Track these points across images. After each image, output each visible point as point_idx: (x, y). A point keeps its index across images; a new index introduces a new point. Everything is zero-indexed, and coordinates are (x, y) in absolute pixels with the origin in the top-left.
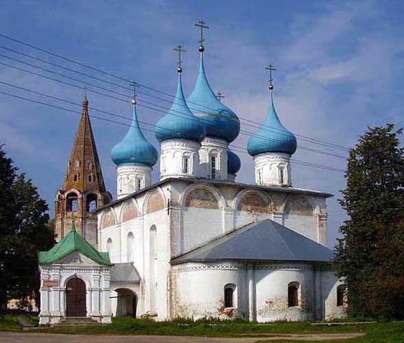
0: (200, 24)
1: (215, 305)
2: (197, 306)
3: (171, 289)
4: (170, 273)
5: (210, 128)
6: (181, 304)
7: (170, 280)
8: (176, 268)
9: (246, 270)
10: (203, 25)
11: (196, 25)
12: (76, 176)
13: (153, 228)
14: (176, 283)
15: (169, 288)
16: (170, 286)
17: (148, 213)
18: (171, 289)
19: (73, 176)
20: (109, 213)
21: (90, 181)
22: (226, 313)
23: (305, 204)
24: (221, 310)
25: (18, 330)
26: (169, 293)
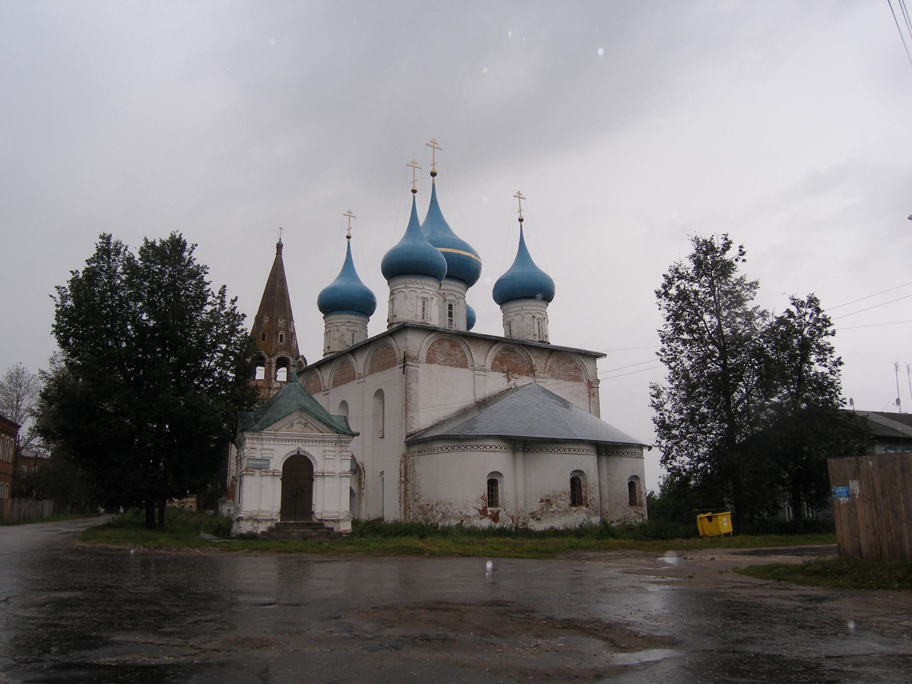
0: (518, 195)
1: (475, 505)
2: (449, 505)
3: (406, 480)
4: (404, 456)
5: (514, 452)
6: (422, 503)
7: (406, 468)
8: (414, 449)
9: (514, 453)
10: (521, 196)
11: (514, 196)
12: (264, 335)
13: (380, 394)
14: (414, 472)
15: (403, 479)
16: (405, 476)
17: (372, 372)
18: (406, 480)
19: (261, 334)
20: (313, 377)
21: (281, 341)
22: (490, 517)
23: (572, 365)
24: (483, 512)
25: (295, 340)
26: (403, 486)
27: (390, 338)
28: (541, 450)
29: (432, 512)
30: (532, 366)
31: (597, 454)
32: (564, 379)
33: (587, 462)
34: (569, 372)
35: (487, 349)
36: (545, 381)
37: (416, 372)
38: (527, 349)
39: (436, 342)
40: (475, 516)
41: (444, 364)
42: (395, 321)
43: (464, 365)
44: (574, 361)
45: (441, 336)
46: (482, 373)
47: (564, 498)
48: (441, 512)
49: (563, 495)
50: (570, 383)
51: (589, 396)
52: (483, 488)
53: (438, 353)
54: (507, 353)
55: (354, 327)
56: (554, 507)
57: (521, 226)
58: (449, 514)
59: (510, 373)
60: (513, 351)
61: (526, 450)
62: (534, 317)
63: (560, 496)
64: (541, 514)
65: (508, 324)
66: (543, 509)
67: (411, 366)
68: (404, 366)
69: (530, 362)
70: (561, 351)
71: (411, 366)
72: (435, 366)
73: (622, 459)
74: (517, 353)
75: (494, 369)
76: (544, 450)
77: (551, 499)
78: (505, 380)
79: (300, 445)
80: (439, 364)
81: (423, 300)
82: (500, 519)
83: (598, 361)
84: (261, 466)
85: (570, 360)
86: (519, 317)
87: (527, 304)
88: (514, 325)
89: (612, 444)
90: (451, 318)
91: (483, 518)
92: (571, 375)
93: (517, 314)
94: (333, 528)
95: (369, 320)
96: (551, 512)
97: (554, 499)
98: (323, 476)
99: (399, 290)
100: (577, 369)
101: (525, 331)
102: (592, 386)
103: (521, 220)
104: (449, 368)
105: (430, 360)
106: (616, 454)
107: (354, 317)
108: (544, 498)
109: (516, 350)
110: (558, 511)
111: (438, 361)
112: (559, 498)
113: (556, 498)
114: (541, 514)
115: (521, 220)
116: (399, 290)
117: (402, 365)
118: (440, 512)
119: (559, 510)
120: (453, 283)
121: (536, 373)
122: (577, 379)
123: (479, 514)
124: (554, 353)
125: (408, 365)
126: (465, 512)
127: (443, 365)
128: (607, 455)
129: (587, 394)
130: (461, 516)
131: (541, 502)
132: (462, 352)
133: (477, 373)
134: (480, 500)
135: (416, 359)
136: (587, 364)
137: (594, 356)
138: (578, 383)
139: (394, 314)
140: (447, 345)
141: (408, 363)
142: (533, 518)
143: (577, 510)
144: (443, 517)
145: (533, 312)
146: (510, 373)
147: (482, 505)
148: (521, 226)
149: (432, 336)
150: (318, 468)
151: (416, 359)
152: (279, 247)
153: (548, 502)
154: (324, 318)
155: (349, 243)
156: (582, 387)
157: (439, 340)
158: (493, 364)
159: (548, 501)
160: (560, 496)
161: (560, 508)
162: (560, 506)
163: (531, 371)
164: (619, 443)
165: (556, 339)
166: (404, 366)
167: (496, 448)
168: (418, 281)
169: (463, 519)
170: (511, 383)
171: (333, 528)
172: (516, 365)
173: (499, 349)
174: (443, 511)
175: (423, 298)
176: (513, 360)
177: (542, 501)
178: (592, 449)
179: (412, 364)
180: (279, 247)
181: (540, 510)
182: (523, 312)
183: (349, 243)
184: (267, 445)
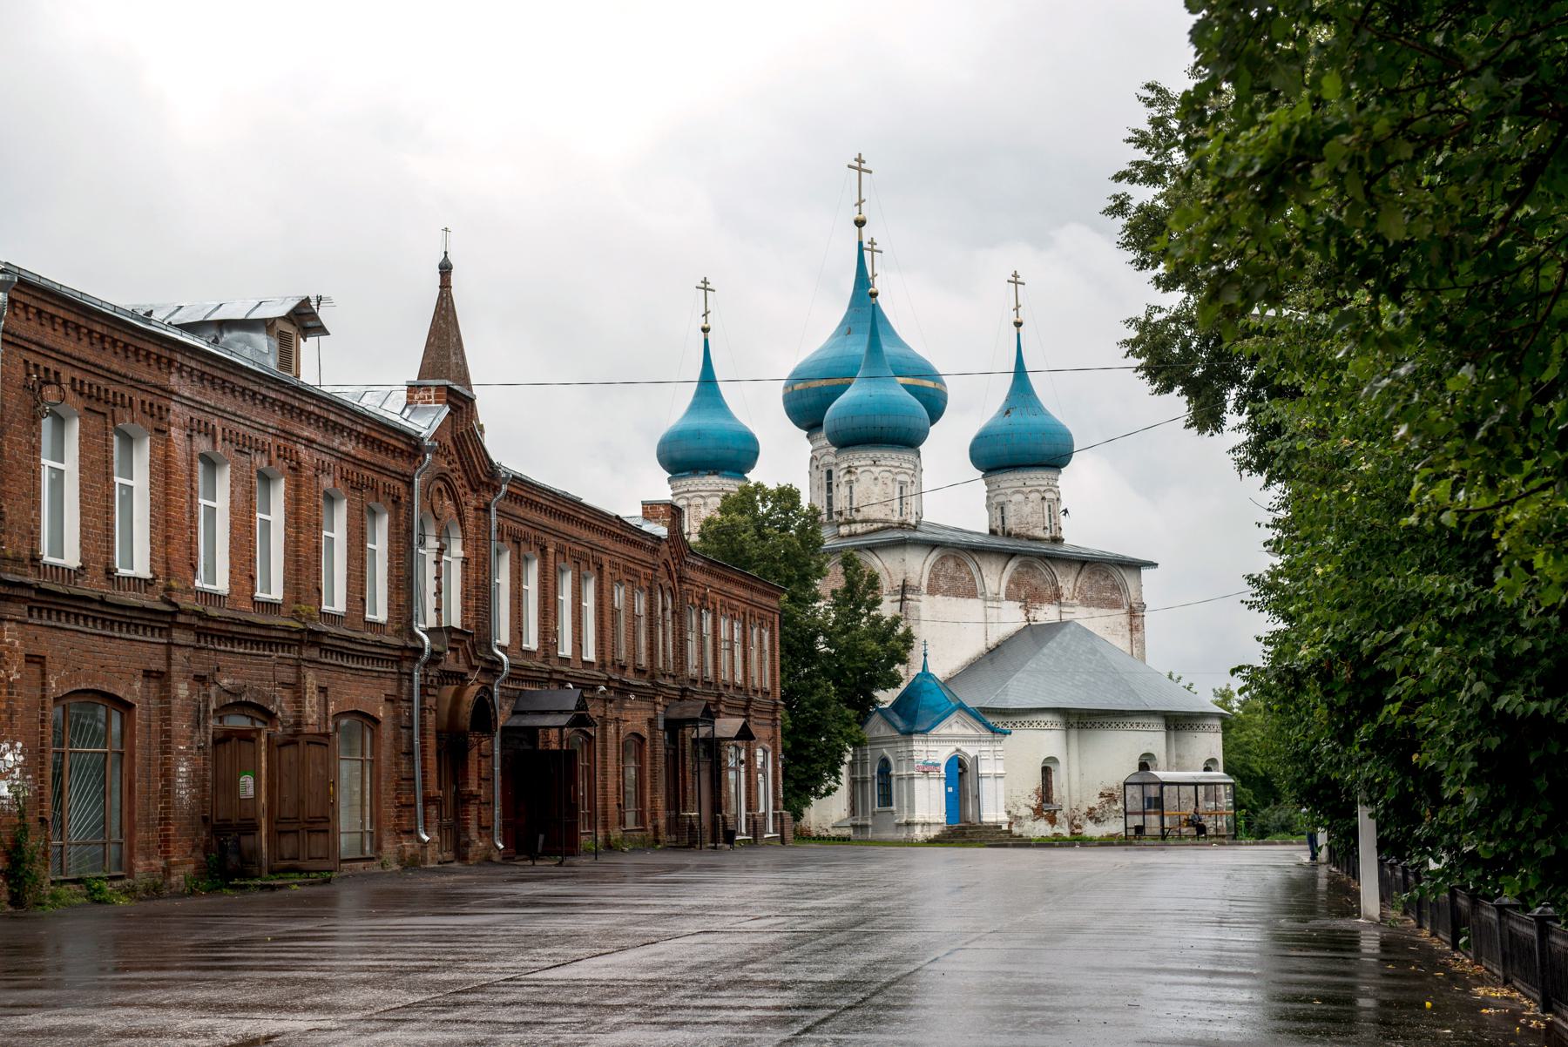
1: (1029, 802)
27: (870, 554)
30: (1058, 589)
33: (1153, 740)
35: (1000, 567)
36: (1072, 610)
37: (918, 609)
40: (1027, 817)
43: (972, 594)
45: (945, 552)
46: (995, 604)
50: (1105, 611)
51: (1131, 630)
52: (1036, 781)
57: (1018, 335)
60: (1031, 566)
62: (1043, 498)
65: (997, 507)
69: (1055, 583)
72: (938, 597)
73: (1199, 735)
75: (1009, 597)
79: (959, 745)
83: (1145, 572)
84: (928, 769)
86: (1019, 497)
87: (1032, 475)
88: (1010, 510)
93: (1017, 492)
100: (1115, 588)
101: (1025, 513)
102: (1135, 613)
103: (1018, 324)
105: (932, 590)
107: (730, 482)
108: (1106, 792)
115: (1018, 324)
117: (899, 597)
121: (1063, 600)
122: (1115, 605)
128: (1176, 729)
129: (1128, 627)
132: (970, 573)
133: (989, 604)
135: (917, 590)
136: (1129, 579)
137: (1135, 566)
139: (855, 505)
140: (951, 564)
141: (909, 596)
142: (1091, 819)
145: (1042, 489)
148: (1018, 335)
151: (917, 590)
152: (445, 269)
154: (670, 480)
155: (706, 341)
156: (1120, 617)
158: (1008, 588)
159: (1110, 795)
163: (1057, 597)
165: (1078, 535)
166: (902, 601)
168: (894, 456)
175: (900, 482)
176: (1033, 581)
177: (1102, 795)
178: (1158, 724)
179: (914, 597)
180: (445, 269)
182: (1027, 490)
183: (706, 341)
184: (932, 747)
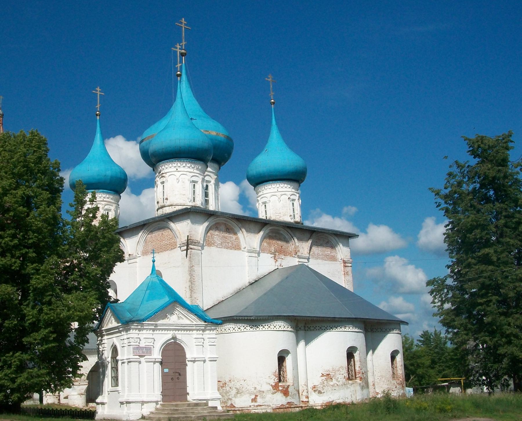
28: (321, 328)
29: (224, 388)
31: (365, 331)
32: (322, 259)
34: (326, 252)
38: (292, 231)
39: (213, 225)
41: (221, 246)
42: (167, 204)
44: (331, 242)
47: (342, 373)
48: (236, 388)
49: (341, 370)
53: (215, 236)
54: (274, 235)
55: (109, 206)
56: (334, 381)
58: (243, 389)
59: (277, 254)
61: (307, 328)
63: (339, 371)
64: (322, 388)
66: (324, 383)
67: (194, 249)
68: (187, 250)
70: (322, 232)
71: (194, 249)
74: (282, 234)
76: (323, 328)
77: (331, 373)
78: (273, 261)
80: (217, 247)
81: (193, 184)
82: (290, 394)
85: (327, 241)
89: (376, 321)
90: (206, 198)
91: (276, 392)
92: (327, 255)
94: (217, 407)
95: (120, 198)
96: (331, 385)
97: (333, 374)
98: (194, 361)
99: (171, 173)
104: (225, 250)
106: (379, 330)
108: (325, 373)
109: (281, 232)
110: (337, 385)
111: (216, 244)
112: (337, 373)
113: (335, 373)
114: (322, 388)
116: (171, 173)
117: (185, 247)
118: (234, 388)
119: (338, 383)
120: (270, 187)
123: (272, 389)
124: (314, 234)
125: (191, 249)
126: (259, 388)
127: (220, 247)
128: (372, 331)
130: (255, 391)
131: (322, 376)
134: (273, 376)
138: (334, 262)
142: (315, 391)
143: (353, 383)
144: (238, 393)
146: (277, 254)
147: (274, 380)
149: (211, 219)
150: (189, 356)
153: (328, 376)
157: (216, 224)
160: (339, 371)
161: (339, 382)
162: (339, 380)
164: (239, 292)
166: (187, 250)
167: (280, 327)
169: (257, 394)
170: (278, 263)
171: (217, 407)
172: (282, 247)
173: (267, 231)
174: (238, 387)
177: (323, 375)
181: (321, 384)
